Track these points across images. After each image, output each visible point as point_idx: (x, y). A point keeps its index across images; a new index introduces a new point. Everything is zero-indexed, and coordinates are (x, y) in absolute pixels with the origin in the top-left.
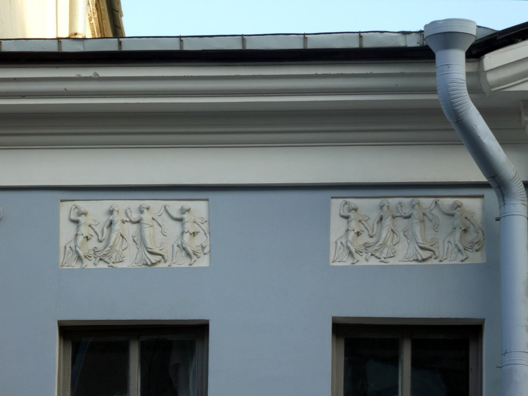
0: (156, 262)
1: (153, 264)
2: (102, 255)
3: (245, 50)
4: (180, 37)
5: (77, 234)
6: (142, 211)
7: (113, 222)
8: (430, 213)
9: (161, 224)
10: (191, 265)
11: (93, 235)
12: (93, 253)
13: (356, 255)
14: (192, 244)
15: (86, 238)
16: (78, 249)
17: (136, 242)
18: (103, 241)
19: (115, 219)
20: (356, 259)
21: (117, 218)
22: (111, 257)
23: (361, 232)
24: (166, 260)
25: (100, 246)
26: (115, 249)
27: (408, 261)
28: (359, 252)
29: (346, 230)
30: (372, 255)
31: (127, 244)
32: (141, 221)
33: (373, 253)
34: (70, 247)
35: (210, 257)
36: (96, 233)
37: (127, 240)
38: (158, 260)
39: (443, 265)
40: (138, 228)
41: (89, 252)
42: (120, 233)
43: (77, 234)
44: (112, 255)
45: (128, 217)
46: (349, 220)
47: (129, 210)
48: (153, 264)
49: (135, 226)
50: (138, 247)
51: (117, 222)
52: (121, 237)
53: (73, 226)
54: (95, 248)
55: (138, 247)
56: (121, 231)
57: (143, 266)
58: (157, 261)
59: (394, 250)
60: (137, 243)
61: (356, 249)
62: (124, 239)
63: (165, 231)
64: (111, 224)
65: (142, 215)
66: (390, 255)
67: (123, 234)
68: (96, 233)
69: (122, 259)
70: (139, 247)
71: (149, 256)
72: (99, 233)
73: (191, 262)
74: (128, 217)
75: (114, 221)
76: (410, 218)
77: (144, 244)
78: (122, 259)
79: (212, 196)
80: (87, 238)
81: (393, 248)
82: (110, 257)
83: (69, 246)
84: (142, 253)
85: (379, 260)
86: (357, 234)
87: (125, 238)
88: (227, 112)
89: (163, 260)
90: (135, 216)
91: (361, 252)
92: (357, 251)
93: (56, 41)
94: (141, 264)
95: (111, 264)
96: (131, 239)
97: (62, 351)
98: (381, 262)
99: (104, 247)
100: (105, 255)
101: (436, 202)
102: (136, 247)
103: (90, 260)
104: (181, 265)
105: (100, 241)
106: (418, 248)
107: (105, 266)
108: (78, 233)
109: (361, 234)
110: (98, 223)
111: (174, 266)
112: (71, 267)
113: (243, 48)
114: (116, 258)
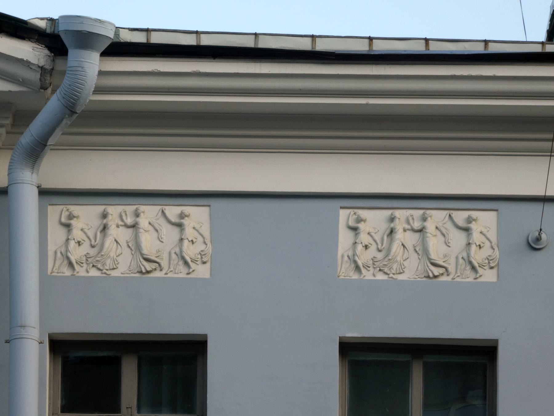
0: (152, 269)
1: (435, 277)
2: (95, 261)
3: (257, 48)
4: (256, 34)
5: (68, 239)
6: (137, 214)
7: (393, 231)
8: (443, 226)
9: (158, 229)
10: (476, 279)
11: (371, 243)
12: (372, 263)
13: (363, 271)
14: (477, 257)
15: (78, 243)
16: (356, 258)
17: (418, 252)
18: (382, 250)
19: (396, 227)
20: (479, 274)
21: (399, 226)
22: (391, 268)
23: (370, 245)
24: (163, 268)
25: (92, 252)
26: (395, 260)
27: (132, 273)
28: (80, 263)
29: (354, 243)
30: (380, 270)
31: (409, 254)
32: (136, 225)
33: (381, 268)
34: (348, 256)
35: (498, 271)
36: (375, 241)
37: (121, 246)
38: (441, 272)
39: (190, 278)
40: (132, 235)
41: (368, 262)
42: (402, 242)
43: (68, 239)
44: (392, 265)
45: (122, 220)
46: (358, 232)
47: (411, 217)
48: (435, 277)
49: (417, 235)
50: (420, 257)
51: (111, 226)
52: (402, 247)
53: (351, 234)
54: (374, 257)
55: (420, 257)
56: (402, 240)
57: (424, 279)
58: (440, 274)
59: (117, 261)
60: (418, 254)
61: (363, 263)
62: (405, 249)
63: (449, 241)
64: (392, 232)
65: (138, 219)
66: (400, 271)
67: (117, 239)
68: (375, 241)
69: (116, 266)
70: (421, 258)
71: (145, 263)
72: (378, 242)
73: (476, 276)
74: (122, 220)
75: (395, 229)
76: (422, 232)
77: (427, 254)
78: (116, 266)
79: (214, 202)
80: (366, 247)
81: (117, 259)
82: (390, 267)
83: (174, 252)
84: (424, 263)
85: (100, 272)
86: (365, 247)
87: (406, 249)
88: (330, 115)
89: (446, 274)
90: (417, 225)
91: (369, 267)
92: (78, 262)
93: (254, 36)
94: (423, 276)
95: (391, 275)
96: (126, 245)
97: (52, 369)
98: (102, 273)
99: (385, 257)
100: (385, 265)
101: (450, 215)
102: (417, 257)
103: (369, 271)
104: (465, 279)
105: (93, 247)
106: (142, 260)
107: (385, 277)
108: (357, 241)
109: (83, 243)
110: (377, 231)
111: (458, 279)
112: (348, 278)
113: (312, 48)
114: (110, 265)
